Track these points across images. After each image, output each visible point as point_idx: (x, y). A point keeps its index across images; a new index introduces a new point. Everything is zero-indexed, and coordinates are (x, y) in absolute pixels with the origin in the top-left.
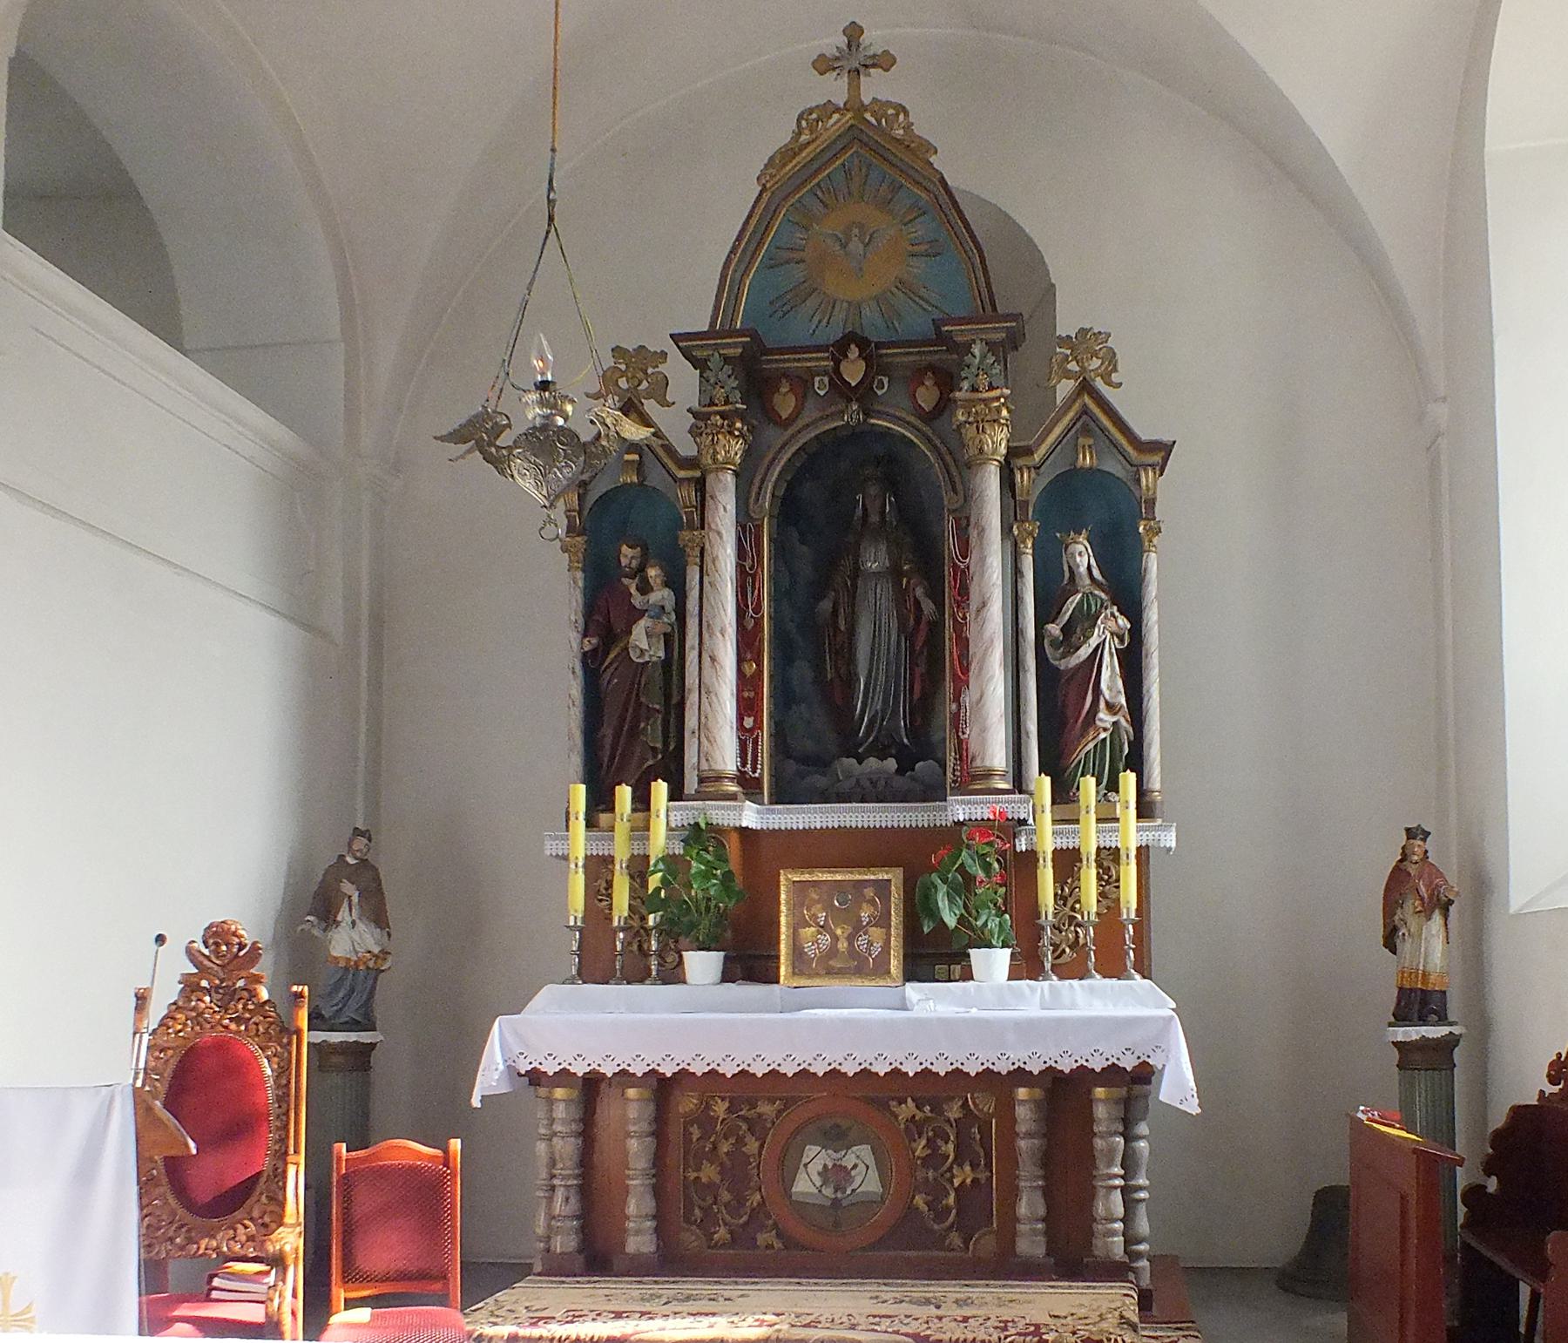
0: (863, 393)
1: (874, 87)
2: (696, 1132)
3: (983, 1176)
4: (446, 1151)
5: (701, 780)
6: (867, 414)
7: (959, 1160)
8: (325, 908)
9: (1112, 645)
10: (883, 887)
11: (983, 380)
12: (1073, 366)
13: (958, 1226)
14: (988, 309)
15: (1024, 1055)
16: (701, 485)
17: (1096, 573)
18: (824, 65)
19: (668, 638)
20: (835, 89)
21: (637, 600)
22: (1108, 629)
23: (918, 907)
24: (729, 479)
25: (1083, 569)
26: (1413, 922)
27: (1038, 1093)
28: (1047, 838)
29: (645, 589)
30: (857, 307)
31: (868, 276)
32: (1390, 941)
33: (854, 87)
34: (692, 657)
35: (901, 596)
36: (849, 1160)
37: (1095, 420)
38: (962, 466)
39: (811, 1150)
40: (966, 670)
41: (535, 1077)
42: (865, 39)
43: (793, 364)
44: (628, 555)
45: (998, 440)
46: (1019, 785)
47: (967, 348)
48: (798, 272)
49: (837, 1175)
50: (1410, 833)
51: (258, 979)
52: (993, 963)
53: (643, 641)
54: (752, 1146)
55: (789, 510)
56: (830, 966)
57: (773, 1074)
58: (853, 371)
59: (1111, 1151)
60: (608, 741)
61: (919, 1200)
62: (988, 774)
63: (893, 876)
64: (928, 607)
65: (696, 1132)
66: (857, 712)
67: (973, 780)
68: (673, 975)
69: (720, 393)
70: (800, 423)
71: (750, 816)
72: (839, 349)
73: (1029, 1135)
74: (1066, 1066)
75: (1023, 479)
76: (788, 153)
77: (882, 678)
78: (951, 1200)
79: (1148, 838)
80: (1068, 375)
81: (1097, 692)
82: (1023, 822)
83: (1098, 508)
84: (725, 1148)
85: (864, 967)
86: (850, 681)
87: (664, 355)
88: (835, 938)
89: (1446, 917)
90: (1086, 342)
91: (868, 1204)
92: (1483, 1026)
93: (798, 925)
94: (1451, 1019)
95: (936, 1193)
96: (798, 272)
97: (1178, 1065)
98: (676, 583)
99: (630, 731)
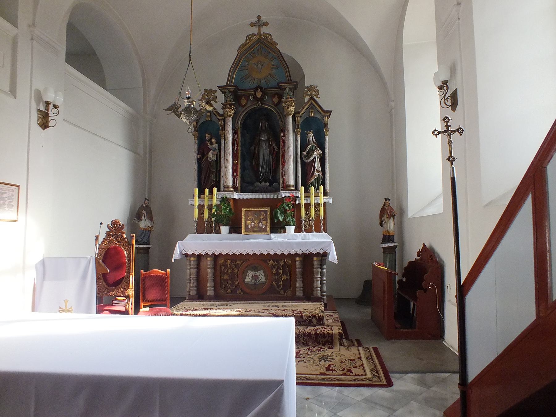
0: (261, 100)
1: (264, 30)
2: (223, 268)
3: (288, 278)
4: (166, 272)
5: (224, 188)
6: (262, 104)
7: (283, 274)
8: (139, 216)
9: (318, 157)
10: (266, 212)
11: (289, 96)
12: (309, 93)
13: (283, 289)
14: (290, 80)
15: (312, 250)
16: (224, 120)
17: (314, 140)
18: (252, 25)
19: (217, 155)
20: (255, 30)
21: (210, 147)
22: (317, 154)
23: (274, 216)
24: (231, 119)
25: (311, 140)
26: (386, 220)
27: (301, 259)
28: (303, 201)
29: (212, 144)
30: (259, 80)
31: (262, 73)
32: (381, 224)
33: (259, 30)
34: (222, 159)
35: (270, 146)
36: (258, 274)
37: (314, 106)
38: (284, 116)
39: (249, 272)
40: (285, 162)
41: (186, 255)
42: (262, 19)
43: (245, 93)
44: (208, 136)
45: (292, 110)
46: (297, 188)
47: (285, 89)
48: (247, 72)
49: (255, 277)
50: (386, 200)
51: (123, 233)
52: (291, 229)
53: (211, 156)
54: (236, 271)
55: (244, 126)
56: (254, 230)
57: (269, 254)
58: (259, 95)
59: (318, 272)
60: (203, 178)
61: (274, 283)
62: (290, 186)
63: (268, 209)
64: (276, 148)
65: (223, 268)
66: (259, 171)
67: (286, 187)
68: (218, 232)
69: (229, 99)
70: (247, 106)
71: (235, 196)
72: (256, 89)
73: (299, 268)
74: (307, 252)
75: (298, 119)
76: (244, 45)
77: (265, 164)
78: (281, 283)
79: (326, 201)
80: (308, 95)
81: (314, 167)
82: (298, 197)
83: (315, 125)
84: (230, 271)
85: (261, 230)
86: (258, 165)
87: (216, 91)
88: (255, 223)
89: (394, 219)
90: (312, 88)
91: (262, 284)
92: (402, 243)
93: (246, 220)
94: (395, 241)
95: (278, 281)
96: (247, 72)
97: (333, 252)
98: (219, 143)
99: (208, 176)
